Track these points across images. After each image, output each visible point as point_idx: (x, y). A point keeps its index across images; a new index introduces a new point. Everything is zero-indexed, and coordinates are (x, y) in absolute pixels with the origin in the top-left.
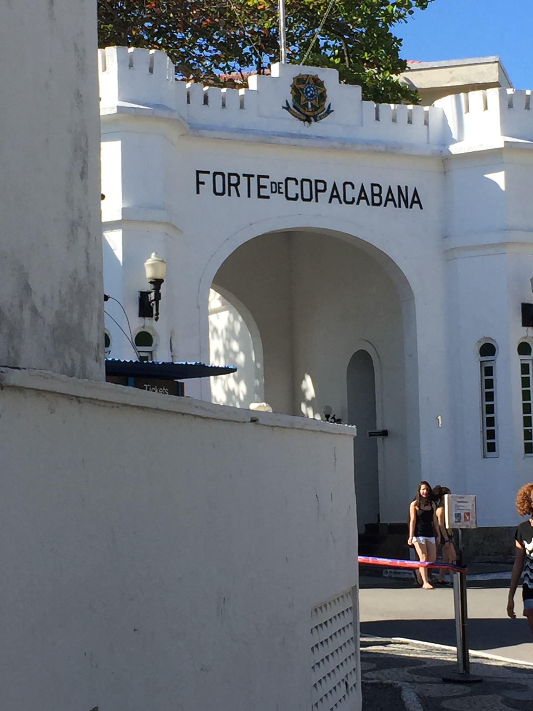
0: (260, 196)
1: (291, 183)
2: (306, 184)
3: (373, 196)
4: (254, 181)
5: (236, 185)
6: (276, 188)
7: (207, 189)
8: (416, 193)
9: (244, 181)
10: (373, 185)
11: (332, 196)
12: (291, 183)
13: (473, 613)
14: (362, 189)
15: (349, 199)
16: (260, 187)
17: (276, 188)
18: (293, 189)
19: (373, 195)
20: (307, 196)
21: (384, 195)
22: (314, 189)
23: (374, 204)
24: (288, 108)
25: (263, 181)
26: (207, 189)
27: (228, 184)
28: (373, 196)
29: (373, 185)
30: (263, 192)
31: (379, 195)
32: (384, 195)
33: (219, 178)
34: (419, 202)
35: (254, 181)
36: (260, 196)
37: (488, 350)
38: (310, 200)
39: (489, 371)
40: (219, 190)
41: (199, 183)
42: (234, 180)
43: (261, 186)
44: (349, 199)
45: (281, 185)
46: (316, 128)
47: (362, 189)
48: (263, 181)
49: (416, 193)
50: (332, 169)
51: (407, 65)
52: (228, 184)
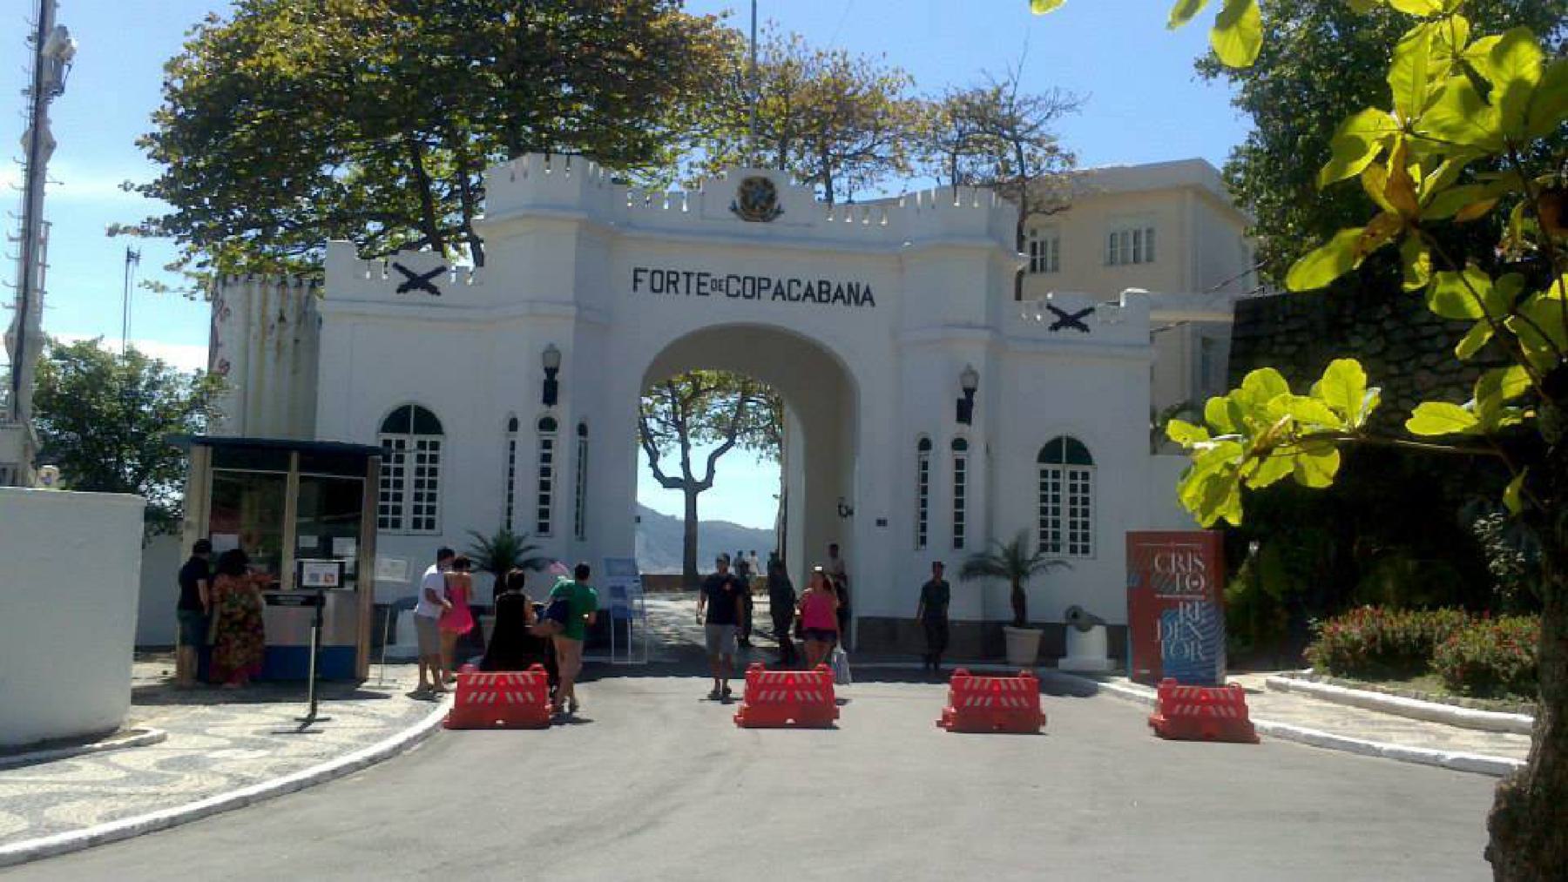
0: (699, 293)
1: (733, 282)
2: (749, 282)
3: (821, 293)
4: (693, 280)
5: (674, 283)
6: (717, 285)
7: (644, 286)
8: (868, 290)
9: (683, 278)
10: (820, 283)
11: (776, 293)
12: (733, 282)
13: (742, 695)
14: (810, 287)
15: (794, 295)
16: (699, 284)
17: (717, 285)
18: (735, 286)
19: (820, 292)
20: (749, 293)
21: (832, 293)
22: (756, 287)
23: (820, 300)
24: (734, 209)
25: (703, 279)
26: (644, 286)
27: (668, 282)
28: (821, 293)
29: (820, 283)
30: (703, 289)
31: (828, 292)
32: (832, 293)
33: (657, 277)
34: (871, 299)
35: (693, 280)
36: (699, 293)
37: (925, 445)
38: (661, 290)
39: (925, 466)
40: (657, 287)
41: (636, 280)
42: (673, 278)
43: (700, 283)
44: (794, 295)
45: (640, 275)
46: (778, 225)
47: (810, 287)
48: (703, 279)
49: (868, 290)
50: (777, 267)
51: (1554, 367)
52: (668, 282)
